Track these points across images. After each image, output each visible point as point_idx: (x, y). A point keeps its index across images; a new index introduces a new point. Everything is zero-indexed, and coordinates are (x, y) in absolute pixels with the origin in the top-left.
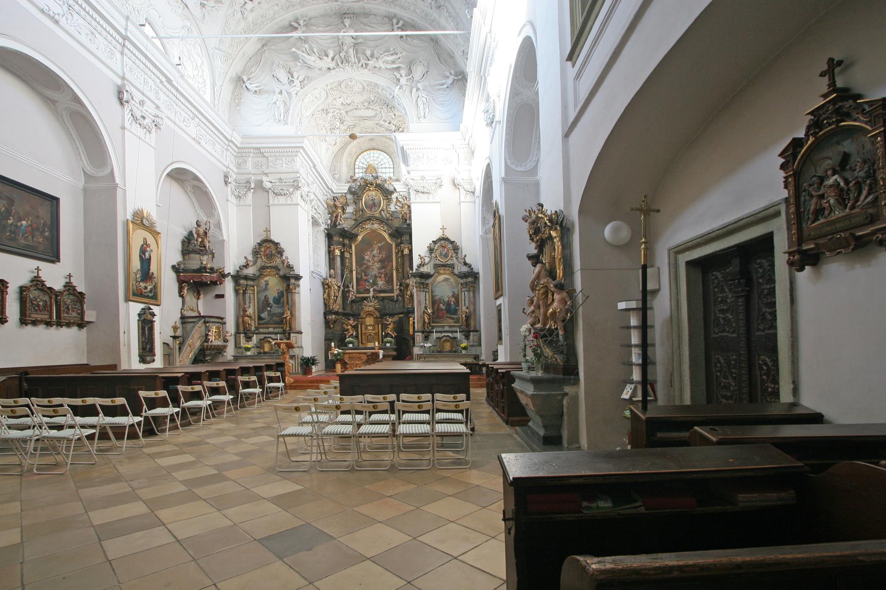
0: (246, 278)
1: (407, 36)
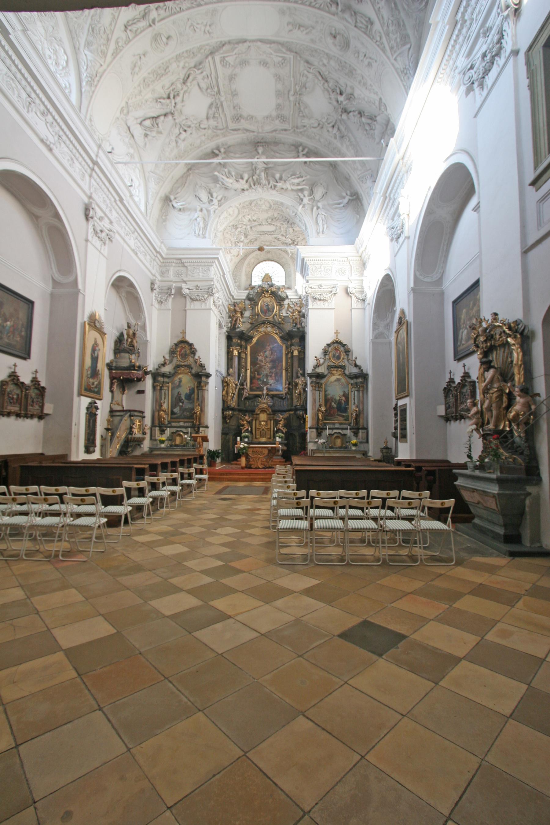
0: (163, 375)
1: (310, 162)
